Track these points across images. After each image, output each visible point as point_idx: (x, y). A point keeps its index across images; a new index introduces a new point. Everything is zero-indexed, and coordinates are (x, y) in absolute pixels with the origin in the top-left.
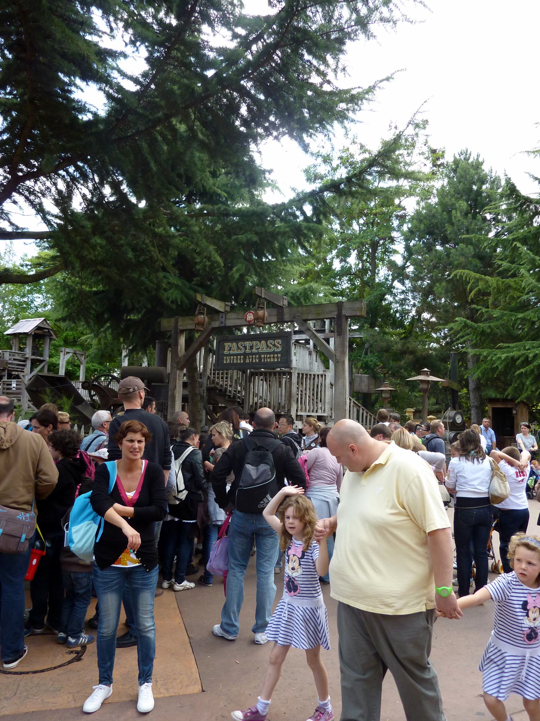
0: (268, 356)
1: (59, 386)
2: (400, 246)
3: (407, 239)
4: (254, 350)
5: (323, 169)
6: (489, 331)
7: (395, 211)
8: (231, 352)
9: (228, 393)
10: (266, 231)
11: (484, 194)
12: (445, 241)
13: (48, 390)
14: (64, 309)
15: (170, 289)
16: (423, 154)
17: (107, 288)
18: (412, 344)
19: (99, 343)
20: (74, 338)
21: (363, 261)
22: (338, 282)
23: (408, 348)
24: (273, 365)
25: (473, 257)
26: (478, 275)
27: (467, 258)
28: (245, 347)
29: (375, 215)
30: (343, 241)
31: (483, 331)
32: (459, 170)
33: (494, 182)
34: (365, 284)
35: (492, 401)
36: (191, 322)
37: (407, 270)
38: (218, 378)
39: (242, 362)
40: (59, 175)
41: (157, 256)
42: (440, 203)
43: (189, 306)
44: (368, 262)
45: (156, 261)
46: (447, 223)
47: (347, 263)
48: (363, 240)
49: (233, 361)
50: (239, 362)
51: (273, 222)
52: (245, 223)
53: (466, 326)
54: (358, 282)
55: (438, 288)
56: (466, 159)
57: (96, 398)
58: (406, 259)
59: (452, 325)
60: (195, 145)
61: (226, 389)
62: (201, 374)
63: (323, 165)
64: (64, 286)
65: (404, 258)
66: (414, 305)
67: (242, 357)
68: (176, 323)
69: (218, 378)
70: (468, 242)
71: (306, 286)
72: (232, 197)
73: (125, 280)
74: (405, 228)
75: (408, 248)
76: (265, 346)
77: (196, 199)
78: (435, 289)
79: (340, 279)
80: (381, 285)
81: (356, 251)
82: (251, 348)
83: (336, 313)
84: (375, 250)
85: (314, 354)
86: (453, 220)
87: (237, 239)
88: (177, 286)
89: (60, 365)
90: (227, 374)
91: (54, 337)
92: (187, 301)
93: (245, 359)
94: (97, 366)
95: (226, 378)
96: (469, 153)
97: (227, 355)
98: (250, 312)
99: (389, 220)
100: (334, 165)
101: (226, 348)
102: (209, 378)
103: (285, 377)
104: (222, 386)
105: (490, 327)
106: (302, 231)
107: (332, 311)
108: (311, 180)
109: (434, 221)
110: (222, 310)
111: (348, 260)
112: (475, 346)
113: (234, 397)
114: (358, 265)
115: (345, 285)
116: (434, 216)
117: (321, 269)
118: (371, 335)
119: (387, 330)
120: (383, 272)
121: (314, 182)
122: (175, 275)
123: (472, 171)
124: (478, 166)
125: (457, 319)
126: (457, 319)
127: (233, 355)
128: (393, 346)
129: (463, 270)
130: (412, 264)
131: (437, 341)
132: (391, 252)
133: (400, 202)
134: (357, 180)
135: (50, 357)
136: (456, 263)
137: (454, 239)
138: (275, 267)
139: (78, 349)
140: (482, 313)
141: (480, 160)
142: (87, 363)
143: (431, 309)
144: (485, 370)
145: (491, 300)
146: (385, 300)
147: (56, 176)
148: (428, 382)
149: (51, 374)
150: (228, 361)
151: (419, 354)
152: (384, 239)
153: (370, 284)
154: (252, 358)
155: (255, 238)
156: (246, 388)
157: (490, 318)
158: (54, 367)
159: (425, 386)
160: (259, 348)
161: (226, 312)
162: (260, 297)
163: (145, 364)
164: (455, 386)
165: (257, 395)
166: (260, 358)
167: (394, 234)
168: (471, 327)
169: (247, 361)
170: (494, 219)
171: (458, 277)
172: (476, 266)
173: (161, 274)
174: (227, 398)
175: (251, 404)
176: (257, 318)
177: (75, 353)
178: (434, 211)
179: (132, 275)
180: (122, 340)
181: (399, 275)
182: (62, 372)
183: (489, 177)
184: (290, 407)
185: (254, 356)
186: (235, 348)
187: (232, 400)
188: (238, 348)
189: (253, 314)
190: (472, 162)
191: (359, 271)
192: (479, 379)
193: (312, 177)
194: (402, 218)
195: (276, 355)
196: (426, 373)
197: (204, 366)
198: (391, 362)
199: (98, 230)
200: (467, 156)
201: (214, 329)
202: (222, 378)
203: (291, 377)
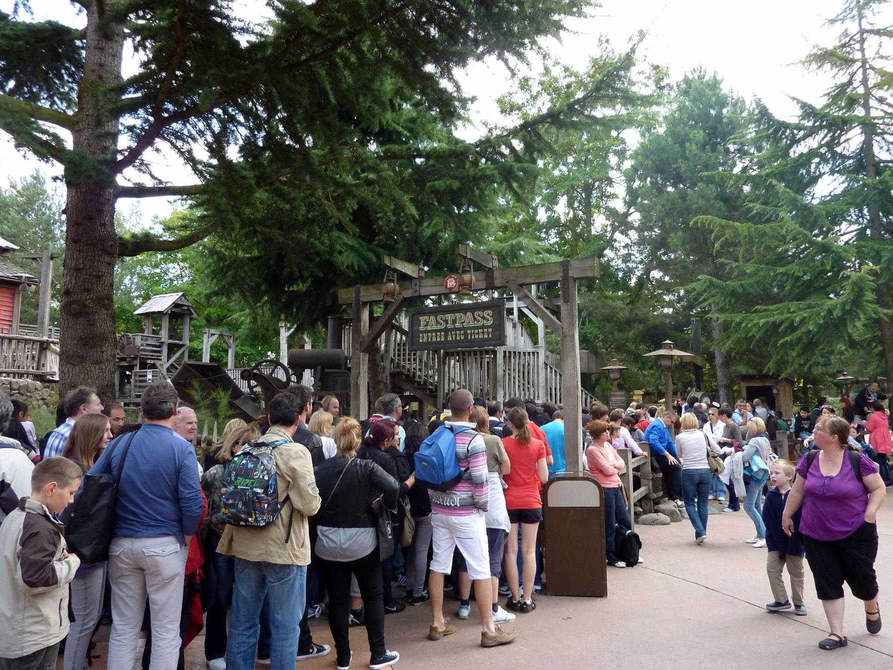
0: (476, 331)
1: (212, 377)
2: (620, 189)
3: (630, 179)
4: (458, 325)
5: (520, 98)
6: (741, 290)
7: (613, 145)
8: (429, 328)
9: (417, 379)
10: (468, 175)
11: (725, 120)
12: (678, 179)
13: (196, 384)
14: (212, 280)
15: (346, 251)
16: (642, 72)
17: (263, 253)
18: (641, 310)
19: (254, 320)
20: (218, 316)
21: (574, 209)
22: (543, 235)
23: (637, 315)
24: (484, 342)
25: (716, 198)
26: (724, 222)
27: (708, 200)
28: (446, 321)
29: (588, 150)
30: (549, 187)
31: (733, 291)
32: (691, 92)
33: (736, 103)
34: (577, 236)
35: (745, 378)
36: (377, 292)
37: (630, 219)
38: (404, 360)
39: (443, 339)
40: (213, 114)
41: (332, 212)
42: (671, 132)
43: (368, 272)
44: (580, 210)
45: (331, 218)
46: (681, 158)
47: (554, 212)
48: (574, 183)
49: (431, 339)
50: (438, 340)
51: (475, 163)
52: (441, 166)
53: (712, 284)
54: (568, 235)
55: (674, 239)
56: (701, 78)
57: (258, 389)
58: (629, 204)
59: (694, 285)
60: (387, 69)
61: (414, 374)
62: (382, 357)
63: (520, 92)
64: (213, 252)
65: (625, 202)
66: (641, 262)
67: (443, 333)
68: (358, 294)
69: (404, 360)
70: (710, 180)
71: (514, 242)
72: (415, 135)
73: (290, 242)
74: (627, 164)
75: (630, 191)
76: (471, 319)
77: (371, 139)
78: (669, 240)
79: (546, 233)
80: (599, 237)
81: (565, 197)
82: (454, 321)
83: (561, 274)
84: (589, 195)
85: (519, 327)
86: (688, 155)
87: (434, 186)
88: (352, 248)
89: (204, 351)
90: (415, 355)
91: (195, 316)
92: (365, 266)
93: (446, 335)
94: (248, 349)
95: (415, 360)
96: (703, 71)
97: (423, 332)
98: (451, 277)
99: (606, 157)
100: (534, 93)
101: (422, 323)
102: (392, 360)
103: (487, 356)
104: (409, 370)
105: (741, 286)
106: (514, 173)
107: (555, 273)
108: (506, 112)
109: (664, 156)
110: (415, 275)
111: (556, 208)
112: (722, 311)
113: (425, 384)
114: (568, 214)
115: (553, 239)
116: (663, 150)
117: (523, 221)
118: (590, 300)
119: (607, 293)
120: (600, 222)
121: (510, 114)
122: (354, 235)
123: (708, 92)
124: (715, 85)
125: (700, 277)
126: (700, 277)
127: (432, 331)
128: (618, 313)
129: (705, 217)
130: (637, 210)
131: (670, 304)
132: (608, 197)
133: (619, 134)
134: (581, 106)
135: (191, 340)
136: (695, 206)
137: (691, 178)
138: (476, 219)
139: (225, 330)
140: (732, 268)
141: (718, 77)
142: (237, 346)
143: (664, 266)
144: (738, 339)
145: (741, 251)
146: (604, 256)
147: (210, 115)
148: (671, 357)
149: (192, 362)
150: (425, 340)
151: (651, 321)
152: (600, 180)
153: (585, 237)
154: (456, 334)
155: (456, 184)
156: (440, 372)
157: (743, 274)
158: (195, 353)
159: (666, 363)
160: (464, 322)
161: (420, 278)
162: (465, 258)
163: (308, 347)
164: (699, 361)
165: (454, 381)
166: (466, 334)
167: (613, 174)
168: (718, 287)
169: (450, 339)
170: (739, 150)
171: (699, 225)
172: (720, 210)
173: (336, 233)
174: (416, 384)
175: (446, 391)
176: (462, 285)
177: (221, 335)
178: (663, 143)
179: (299, 236)
180: (283, 316)
181: (621, 224)
182: (206, 359)
183: (729, 99)
184: (496, 394)
185: (458, 332)
186: (433, 322)
187: (422, 386)
188: (438, 322)
189: (455, 279)
190: (707, 82)
191: (570, 221)
192: (729, 352)
193: (507, 107)
194: (621, 154)
195: (485, 330)
196: (669, 347)
197: (386, 346)
198: (616, 333)
199: (263, 180)
200: (702, 74)
201: (405, 299)
202: (409, 360)
203: (495, 356)
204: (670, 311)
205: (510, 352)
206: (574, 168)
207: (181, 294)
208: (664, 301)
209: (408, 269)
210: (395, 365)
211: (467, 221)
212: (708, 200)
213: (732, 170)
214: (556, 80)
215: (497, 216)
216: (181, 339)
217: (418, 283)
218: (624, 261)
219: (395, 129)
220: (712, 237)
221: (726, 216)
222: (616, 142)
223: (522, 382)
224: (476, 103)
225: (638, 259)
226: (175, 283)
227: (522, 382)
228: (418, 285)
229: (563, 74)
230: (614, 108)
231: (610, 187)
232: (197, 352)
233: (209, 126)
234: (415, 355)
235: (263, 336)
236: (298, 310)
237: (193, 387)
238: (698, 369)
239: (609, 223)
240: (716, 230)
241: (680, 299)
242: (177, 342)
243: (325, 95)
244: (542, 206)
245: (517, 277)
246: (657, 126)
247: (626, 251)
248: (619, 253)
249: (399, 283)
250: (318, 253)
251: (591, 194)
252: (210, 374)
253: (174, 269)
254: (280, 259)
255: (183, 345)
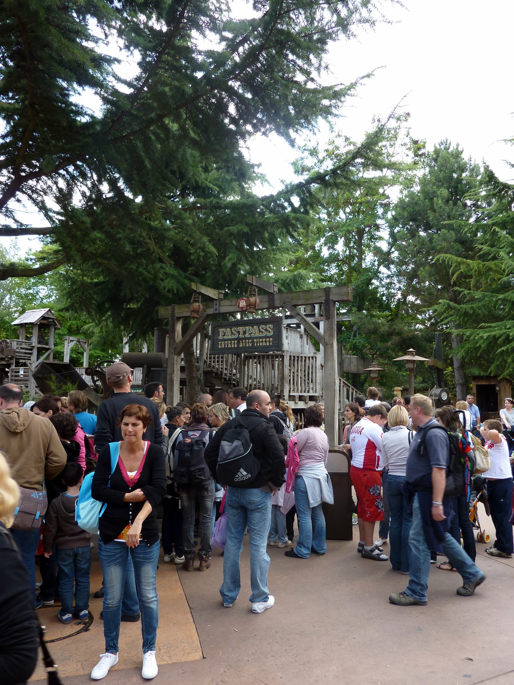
0: (261, 340)
1: (64, 372)
2: (384, 233)
3: (392, 226)
4: (247, 335)
8: (226, 337)
9: (224, 376)
10: (256, 222)
13: (53, 377)
14: (67, 299)
15: (166, 279)
18: (399, 326)
21: (350, 248)
23: (395, 329)
24: (266, 349)
26: (459, 259)
27: (449, 242)
28: (239, 333)
31: (465, 312)
32: (439, 159)
34: (352, 269)
36: (186, 309)
37: (393, 256)
38: (214, 362)
39: (236, 346)
41: (154, 248)
42: (422, 191)
43: (185, 294)
44: (355, 249)
45: (153, 253)
47: (335, 250)
49: (227, 345)
50: (233, 346)
51: (262, 214)
53: (449, 307)
54: (345, 268)
55: (422, 272)
56: (447, 149)
57: (99, 383)
58: (391, 245)
61: (222, 372)
62: (198, 359)
63: (310, 157)
64: (67, 278)
66: (400, 289)
67: (236, 341)
68: (173, 311)
69: (214, 362)
70: (450, 227)
74: (390, 215)
75: (392, 235)
77: (190, 193)
78: (419, 273)
80: (367, 270)
81: (343, 238)
82: (245, 333)
83: (324, 298)
84: (361, 237)
87: (229, 230)
88: (173, 276)
89: (65, 353)
91: (59, 326)
92: (182, 290)
93: (238, 343)
94: (99, 353)
95: (222, 362)
97: (221, 340)
98: (243, 299)
99: (374, 209)
100: (321, 157)
101: (220, 333)
102: (205, 362)
104: (217, 369)
108: (298, 172)
109: (417, 208)
112: (458, 327)
113: (230, 380)
114: (346, 251)
116: (416, 203)
117: (310, 257)
118: (359, 318)
120: (369, 258)
123: (452, 160)
124: (457, 155)
125: (440, 301)
126: (440, 301)
127: (228, 340)
128: (380, 328)
129: (445, 255)
130: (396, 250)
132: (376, 239)
135: (55, 345)
136: (439, 247)
138: (266, 255)
139: (82, 338)
142: (90, 350)
143: (416, 292)
144: (469, 349)
146: (372, 284)
147: (57, 175)
148: (413, 362)
149: (57, 362)
150: (223, 346)
151: (405, 335)
152: (369, 226)
153: (357, 269)
154: (246, 342)
155: (246, 229)
156: (241, 371)
158: (59, 355)
159: (411, 366)
160: (252, 333)
161: (220, 300)
163: (145, 350)
164: (440, 365)
166: (253, 343)
167: (379, 222)
168: (454, 308)
169: (241, 345)
171: (441, 261)
172: (458, 250)
173: (158, 265)
174: (223, 380)
176: (249, 305)
178: (416, 198)
180: (122, 328)
181: (385, 260)
184: (283, 388)
186: (229, 333)
188: (232, 333)
190: (452, 152)
191: (347, 257)
192: (463, 358)
194: (386, 206)
195: (268, 339)
196: (411, 354)
197: (200, 351)
198: (378, 343)
202: (218, 362)
203: (283, 360)
204: (421, 327)
205: (294, 357)
206: (351, 217)
207: (48, 309)
208: (417, 319)
209: (211, 293)
210: (208, 366)
211: (260, 257)
212: (449, 242)
213: (468, 220)
214: (337, 148)
215: (283, 253)
216: (47, 344)
217: (218, 304)
218: (388, 289)
219: (207, 186)
220: (451, 271)
221: (464, 255)
222: (383, 198)
223: (307, 381)
224: (261, 167)
225: (397, 286)
226: (45, 301)
227: (307, 381)
228: (218, 305)
229: (344, 144)
230: (382, 171)
231: (378, 231)
232: (60, 354)
233: (56, 183)
234: (222, 358)
235: (112, 343)
236: (133, 322)
237: (51, 379)
238: (439, 371)
239: (377, 259)
240: (453, 265)
241: (430, 319)
242: (44, 346)
243: (142, 162)
244: (325, 246)
245: (291, 300)
246: (414, 185)
247: (388, 281)
248: (383, 283)
249: (204, 303)
250: (145, 280)
251: (363, 237)
252: (63, 371)
253: (43, 291)
254: (118, 284)
255: (48, 349)
